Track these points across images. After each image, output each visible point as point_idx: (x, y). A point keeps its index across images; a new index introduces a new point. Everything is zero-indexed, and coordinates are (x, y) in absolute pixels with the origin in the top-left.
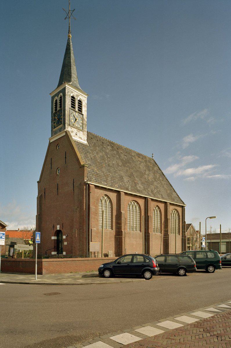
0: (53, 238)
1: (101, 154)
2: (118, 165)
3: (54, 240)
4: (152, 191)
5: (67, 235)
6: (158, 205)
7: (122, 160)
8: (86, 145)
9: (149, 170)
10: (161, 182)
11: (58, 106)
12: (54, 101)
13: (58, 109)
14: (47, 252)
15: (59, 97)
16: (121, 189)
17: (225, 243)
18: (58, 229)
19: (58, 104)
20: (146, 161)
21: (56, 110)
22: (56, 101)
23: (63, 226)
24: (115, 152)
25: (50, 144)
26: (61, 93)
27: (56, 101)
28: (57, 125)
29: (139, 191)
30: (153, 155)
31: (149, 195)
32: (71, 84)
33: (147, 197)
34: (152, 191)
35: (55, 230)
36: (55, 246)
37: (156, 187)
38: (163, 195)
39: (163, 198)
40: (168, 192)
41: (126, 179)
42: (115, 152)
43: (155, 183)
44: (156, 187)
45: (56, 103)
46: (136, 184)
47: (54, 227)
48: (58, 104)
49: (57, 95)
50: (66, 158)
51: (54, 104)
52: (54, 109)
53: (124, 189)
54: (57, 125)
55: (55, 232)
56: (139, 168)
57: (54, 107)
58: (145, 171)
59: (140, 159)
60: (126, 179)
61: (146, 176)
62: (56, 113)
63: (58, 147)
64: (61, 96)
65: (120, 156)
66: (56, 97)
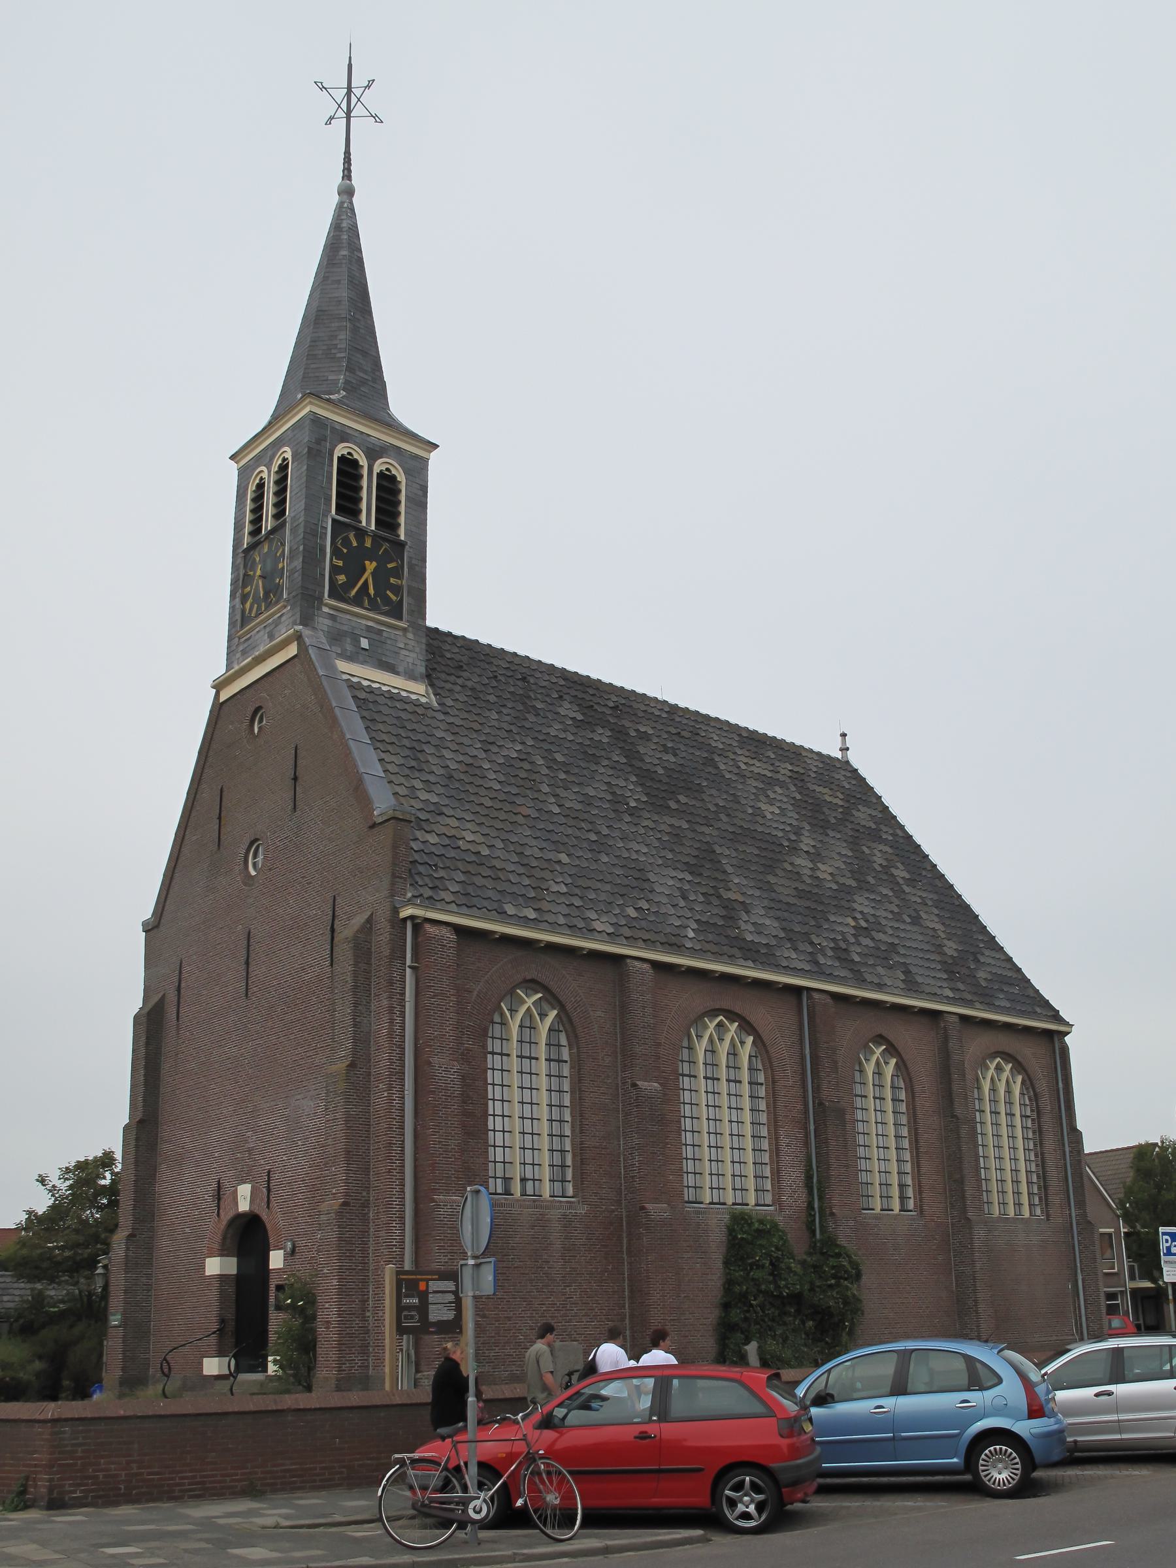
0: (214, 1266)
1: (512, 750)
2: (617, 801)
3: (222, 1278)
4: (842, 954)
5: (289, 1245)
6: (885, 1034)
7: (645, 776)
8: (427, 707)
9: (821, 826)
10: (899, 892)
11: (269, 509)
12: (252, 487)
13: (268, 523)
14: (168, 1358)
15: (275, 468)
16: (631, 940)
17: (908, 1391)
18: (244, 1206)
19: (269, 499)
20: (798, 778)
21: (256, 532)
22: (261, 486)
23: (269, 1190)
24: (603, 735)
25: (218, 711)
26: (284, 445)
27: (261, 486)
28: (259, 608)
29: (751, 953)
30: (844, 742)
31: (820, 972)
32: (339, 401)
33: (809, 989)
34: (842, 954)
35: (226, 1216)
36: (222, 1321)
37: (864, 924)
38: (913, 969)
39: (912, 987)
40: (951, 948)
41: (666, 882)
42: (603, 735)
43: (862, 903)
44: (864, 924)
45: (259, 498)
46: (731, 912)
47: (218, 1196)
48: (269, 499)
49: (263, 458)
50: (295, 779)
51: (249, 505)
52: (247, 528)
53: (649, 943)
54: (259, 608)
55: (224, 1223)
56: (758, 813)
57: (248, 517)
58: (798, 832)
59: (759, 767)
60: (666, 882)
61: (802, 862)
62: (253, 547)
63: (261, 721)
64: (284, 459)
65: (632, 755)
66: (263, 468)
